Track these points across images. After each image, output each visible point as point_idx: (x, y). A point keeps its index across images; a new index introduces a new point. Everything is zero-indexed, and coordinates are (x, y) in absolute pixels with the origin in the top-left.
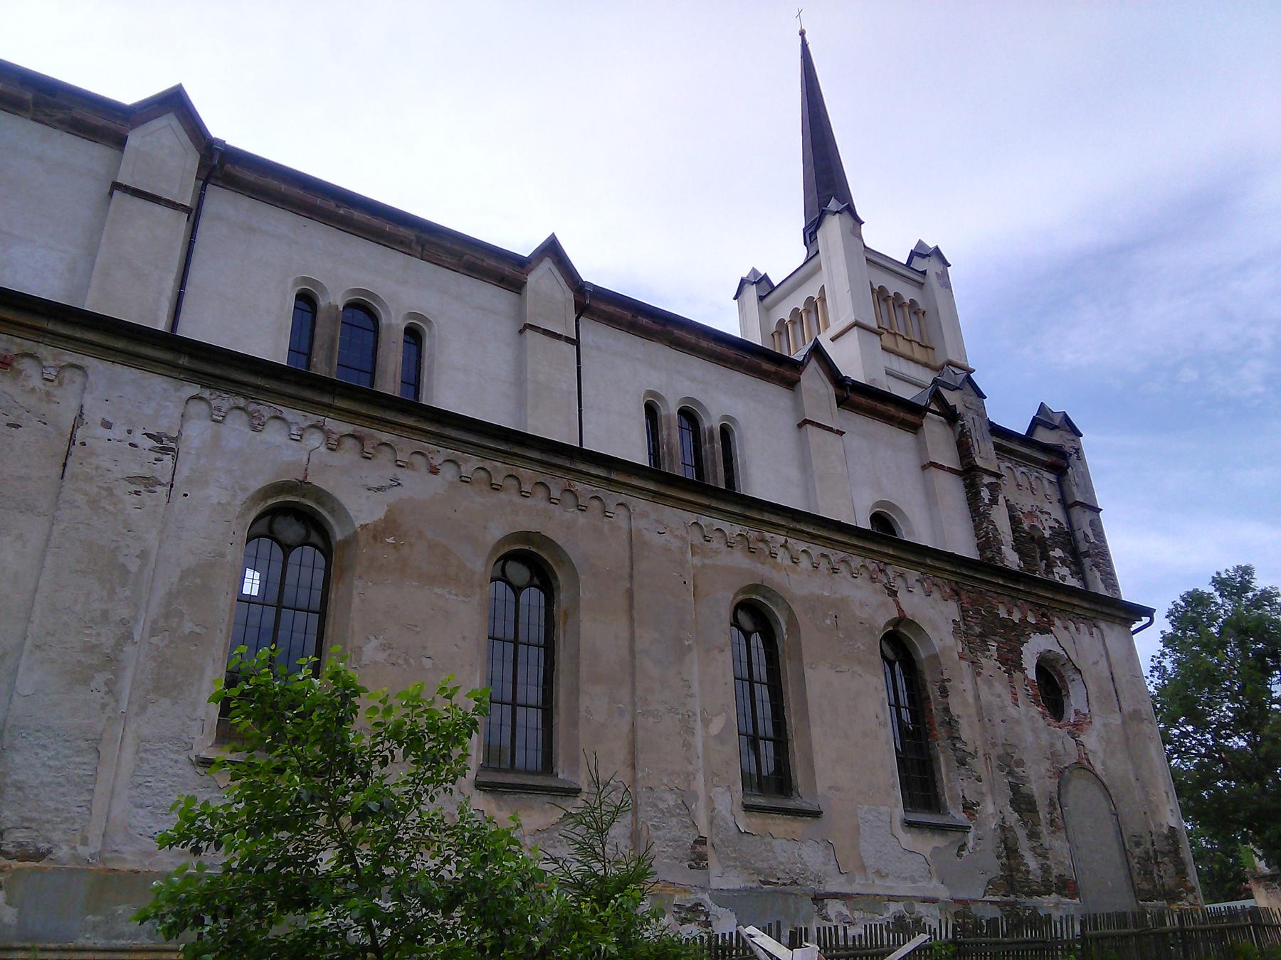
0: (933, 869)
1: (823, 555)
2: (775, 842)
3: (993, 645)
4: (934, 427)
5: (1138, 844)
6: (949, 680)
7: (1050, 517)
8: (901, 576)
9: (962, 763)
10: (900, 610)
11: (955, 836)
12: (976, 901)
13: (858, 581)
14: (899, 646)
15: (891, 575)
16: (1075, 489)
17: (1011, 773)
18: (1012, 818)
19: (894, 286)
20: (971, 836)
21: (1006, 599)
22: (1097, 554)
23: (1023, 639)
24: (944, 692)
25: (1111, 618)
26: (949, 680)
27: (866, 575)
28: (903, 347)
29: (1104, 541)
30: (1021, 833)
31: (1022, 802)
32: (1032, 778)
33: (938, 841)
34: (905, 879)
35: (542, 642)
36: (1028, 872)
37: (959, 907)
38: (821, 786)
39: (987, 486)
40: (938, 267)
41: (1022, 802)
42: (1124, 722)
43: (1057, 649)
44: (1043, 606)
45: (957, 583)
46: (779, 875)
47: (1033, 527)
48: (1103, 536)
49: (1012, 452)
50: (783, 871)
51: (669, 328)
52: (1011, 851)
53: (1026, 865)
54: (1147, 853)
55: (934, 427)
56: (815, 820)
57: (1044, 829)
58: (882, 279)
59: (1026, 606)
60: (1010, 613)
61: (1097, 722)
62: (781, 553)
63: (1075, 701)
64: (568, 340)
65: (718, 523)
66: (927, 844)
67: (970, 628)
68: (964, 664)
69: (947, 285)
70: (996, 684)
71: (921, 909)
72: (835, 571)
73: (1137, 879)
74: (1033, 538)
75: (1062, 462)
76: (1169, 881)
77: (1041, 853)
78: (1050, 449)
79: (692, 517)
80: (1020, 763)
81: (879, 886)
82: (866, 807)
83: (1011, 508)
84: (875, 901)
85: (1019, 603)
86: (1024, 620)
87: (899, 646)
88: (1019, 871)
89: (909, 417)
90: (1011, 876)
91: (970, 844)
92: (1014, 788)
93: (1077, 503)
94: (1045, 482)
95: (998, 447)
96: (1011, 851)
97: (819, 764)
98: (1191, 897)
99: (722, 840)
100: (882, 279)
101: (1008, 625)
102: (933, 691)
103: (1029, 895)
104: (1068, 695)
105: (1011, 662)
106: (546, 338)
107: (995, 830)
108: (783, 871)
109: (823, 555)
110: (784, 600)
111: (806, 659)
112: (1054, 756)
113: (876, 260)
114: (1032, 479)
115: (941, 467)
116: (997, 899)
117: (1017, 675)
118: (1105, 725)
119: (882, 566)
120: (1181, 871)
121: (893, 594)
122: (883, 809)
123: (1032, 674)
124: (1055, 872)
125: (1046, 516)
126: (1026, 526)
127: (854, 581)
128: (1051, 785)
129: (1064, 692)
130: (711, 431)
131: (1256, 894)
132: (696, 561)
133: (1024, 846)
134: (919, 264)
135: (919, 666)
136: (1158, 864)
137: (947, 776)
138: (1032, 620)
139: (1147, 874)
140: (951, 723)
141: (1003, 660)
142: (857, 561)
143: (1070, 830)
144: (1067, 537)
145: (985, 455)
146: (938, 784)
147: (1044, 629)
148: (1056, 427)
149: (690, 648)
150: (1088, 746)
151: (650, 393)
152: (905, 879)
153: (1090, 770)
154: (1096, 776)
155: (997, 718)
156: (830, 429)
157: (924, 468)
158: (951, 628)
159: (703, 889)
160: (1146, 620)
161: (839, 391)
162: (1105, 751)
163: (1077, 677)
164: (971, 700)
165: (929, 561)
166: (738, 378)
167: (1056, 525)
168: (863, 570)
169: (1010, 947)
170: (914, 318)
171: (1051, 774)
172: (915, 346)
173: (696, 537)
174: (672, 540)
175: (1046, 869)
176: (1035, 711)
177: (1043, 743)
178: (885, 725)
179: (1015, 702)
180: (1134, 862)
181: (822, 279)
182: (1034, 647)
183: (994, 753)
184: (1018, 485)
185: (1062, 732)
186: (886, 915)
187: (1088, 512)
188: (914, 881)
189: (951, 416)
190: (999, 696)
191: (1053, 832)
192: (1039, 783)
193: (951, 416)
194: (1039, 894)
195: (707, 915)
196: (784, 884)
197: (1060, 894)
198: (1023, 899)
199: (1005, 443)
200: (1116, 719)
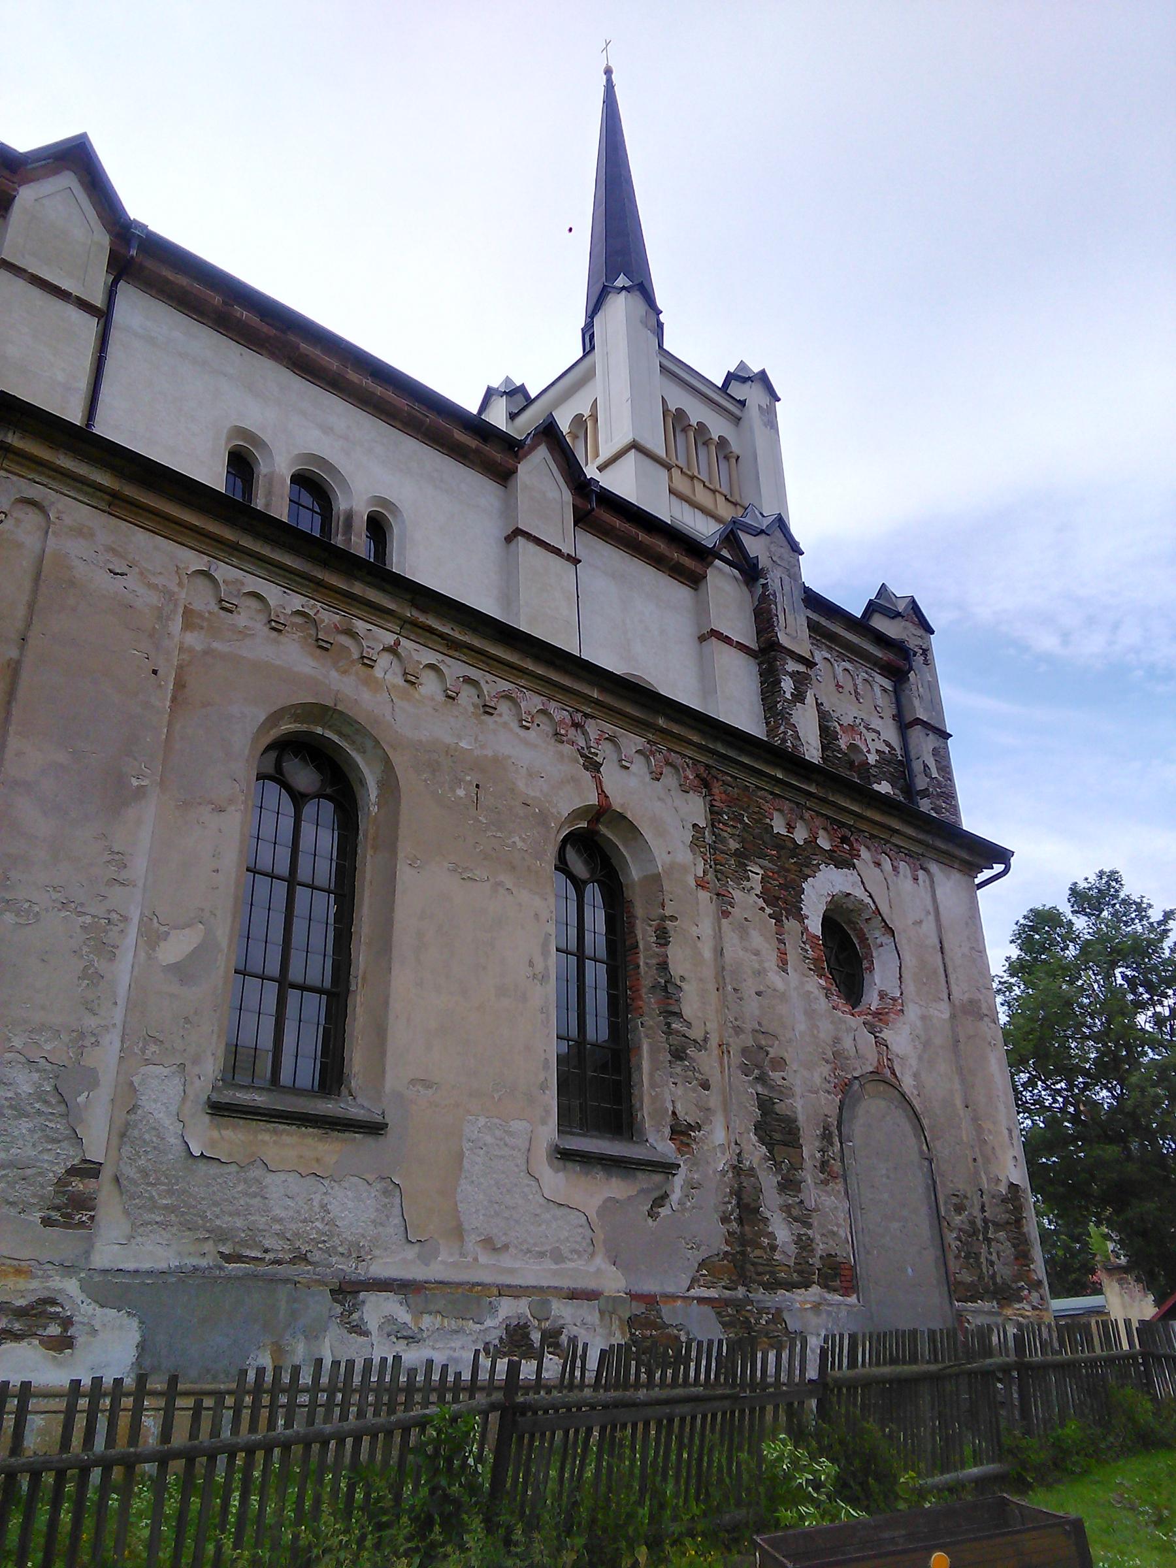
0: (600, 1235)
1: (468, 680)
2: (269, 1179)
3: (756, 873)
4: (722, 581)
5: (959, 1209)
6: (673, 918)
7: (878, 737)
8: (611, 739)
9: (678, 1055)
10: (602, 793)
11: (648, 1180)
12: (674, 1297)
13: (532, 735)
14: (594, 851)
15: (593, 734)
16: (916, 702)
17: (762, 1079)
18: (756, 1153)
19: (697, 413)
20: (678, 1181)
21: (787, 806)
22: (939, 795)
23: (807, 871)
24: (663, 937)
25: (947, 860)
26: (673, 918)
27: (547, 728)
28: (703, 496)
29: (951, 779)
30: (769, 1181)
31: (777, 1130)
32: (798, 1090)
33: (617, 1188)
34: (542, 1254)
35: (328, 984)
36: (773, 1248)
37: (638, 1308)
38: (394, 1080)
39: (792, 675)
40: (765, 400)
41: (777, 1130)
42: (953, 1016)
43: (859, 893)
44: (843, 825)
45: (707, 766)
46: (267, 1243)
47: (853, 747)
48: (950, 773)
49: (832, 637)
50: (280, 1235)
51: (292, 338)
52: (746, 1211)
53: (772, 1236)
54: (972, 1223)
55: (722, 581)
56: (370, 1142)
57: (809, 1176)
58: (679, 399)
59: (818, 822)
60: (790, 828)
61: (912, 1012)
62: (384, 660)
63: (881, 977)
64: (84, 305)
65: (253, 583)
66: (594, 1193)
67: (724, 841)
68: (704, 896)
69: (771, 423)
70: (754, 934)
71: (563, 1312)
72: (488, 710)
73: (953, 1265)
74: (852, 763)
75: (901, 663)
76: (1004, 1271)
77: (800, 1216)
78: (887, 642)
79: (197, 562)
80: (779, 1063)
81: (485, 1269)
82: (482, 1121)
83: (824, 717)
84: (466, 1298)
85: (807, 815)
86: (812, 842)
87: (594, 851)
88: (759, 1246)
89: (687, 561)
90: (743, 1253)
91: (676, 1196)
92: (765, 1105)
93: (918, 721)
94: (877, 689)
95: (813, 627)
96: (746, 1211)
97: (399, 1034)
98: (1035, 1296)
99: (145, 1173)
100: (679, 399)
101: (784, 845)
102: (644, 934)
103: (772, 1286)
104: (871, 969)
105: (783, 901)
106: (35, 292)
107: (724, 1173)
108: (280, 1235)
109: (468, 680)
110: (377, 742)
111: (405, 849)
112: (838, 1058)
113: (675, 371)
114: (859, 681)
115: (727, 640)
116: (712, 1293)
117: (791, 924)
118: (923, 1018)
119: (578, 717)
120: (1023, 1257)
121: (593, 766)
122: (517, 1125)
123: (815, 926)
124: (820, 1248)
125: (874, 736)
126: (843, 743)
127: (522, 732)
128: (828, 1104)
129: (865, 964)
130: (349, 517)
131: (1107, 1289)
132: (193, 639)
133: (771, 1201)
134: (737, 390)
135: (628, 894)
136: (988, 1241)
137: (651, 1075)
138: (824, 843)
139: (971, 1258)
140: (668, 989)
141: (769, 897)
142: (532, 702)
143: (852, 1180)
144: (900, 767)
145: (793, 631)
146: (635, 1091)
147: (844, 862)
148: (899, 615)
149: (140, 793)
150: (894, 1048)
151: (241, 432)
152: (542, 1254)
153: (893, 1084)
154: (903, 1095)
155: (749, 987)
156: (557, 552)
157: (702, 639)
158: (688, 836)
159: (68, 1269)
160: (999, 868)
161: (579, 502)
162: (920, 1058)
163: (886, 939)
164: (707, 954)
165: (661, 722)
166: (411, 446)
167: (887, 750)
168: (541, 719)
169: (649, 1411)
170: (723, 465)
171: (830, 1087)
172: (720, 499)
173: (202, 600)
174: (141, 590)
175: (804, 1245)
176: (815, 984)
177: (822, 1035)
178: (544, 978)
179: (783, 965)
180: (951, 1237)
181: (595, 390)
182: (822, 887)
183: (736, 1044)
184: (838, 685)
185: (855, 1022)
186: (489, 1323)
187: (931, 736)
188: (558, 1257)
189: (750, 572)
190: (757, 953)
191: (825, 1182)
192: (808, 1097)
193: (750, 572)
194: (790, 1286)
195: (67, 1322)
196: (278, 1262)
197: (825, 1286)
198: (759, 1295)
199: (823, 621)
200: (941, 1012)
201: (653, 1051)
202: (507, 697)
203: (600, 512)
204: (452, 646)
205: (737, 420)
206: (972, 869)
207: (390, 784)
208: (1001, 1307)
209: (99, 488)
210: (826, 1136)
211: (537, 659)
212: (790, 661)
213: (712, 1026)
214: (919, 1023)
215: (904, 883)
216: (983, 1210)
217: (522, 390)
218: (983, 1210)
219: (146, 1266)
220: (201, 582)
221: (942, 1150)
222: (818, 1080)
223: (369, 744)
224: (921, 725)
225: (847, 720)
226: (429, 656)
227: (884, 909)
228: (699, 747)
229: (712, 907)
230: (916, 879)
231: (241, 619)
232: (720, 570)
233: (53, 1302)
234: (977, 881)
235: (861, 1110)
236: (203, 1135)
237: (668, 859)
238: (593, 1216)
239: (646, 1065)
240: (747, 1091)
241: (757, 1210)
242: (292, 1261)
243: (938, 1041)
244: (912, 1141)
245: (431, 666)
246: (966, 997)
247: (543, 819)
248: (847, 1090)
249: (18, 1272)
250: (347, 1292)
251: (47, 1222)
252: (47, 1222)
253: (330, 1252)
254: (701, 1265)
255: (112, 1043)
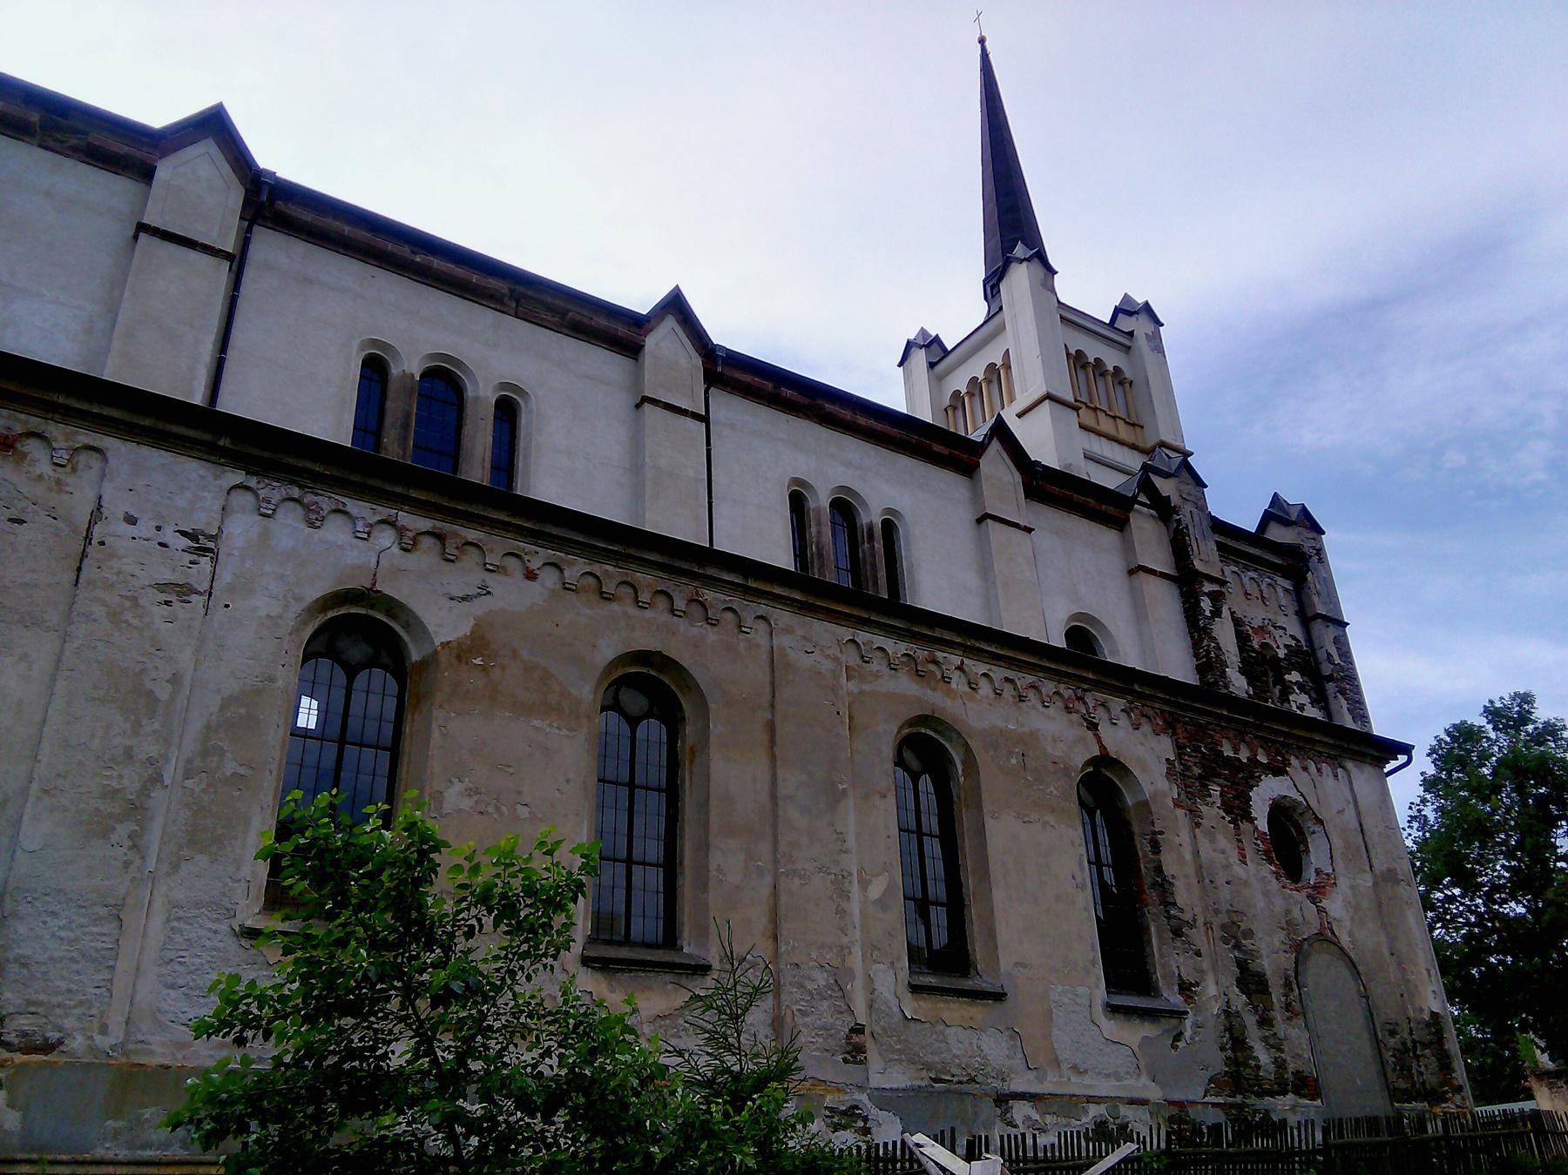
1: (1007, 680)
2: (948, 1031)
3: (1215, 790)
4: (1144, 525)
5: (1393, 1033)
6: (1161, 833)
7: (1286, 633)
9: (1177, 933)
10: (1102, 747)
12: (1194, 1103)
13: (1051, 711)
14: (1102, 787)
15: (1091, 704)
16: (1315, 599)
17: (1237, 946)
18: (1239, 1001)
19: (1094, 350)
20: (1188, 1023)
22: (1343, 679)
24: (1156, 847)
25: (1359, 757)
26: (1161, 833)
27: (1060, 704)
28: (1106, 425)
29: (1352, 663)
30: (1250, 1020)
31: (1251, 982)
32: (1264, 952)
33: (1148, 1030)
34: (1108, 1075)
36: (1258, 1067)
37: (1175, 1111)
39: (1209, 595)
40: (1149, 327)
41: (1251, 982)
42: (1375, 884)
43: (1293, 794)
45: (1171, 713)
46: (954, 1071)
47: (1264, 645)
48: (1350, 657)
50: (959, 1066)
51: (820, 402)
52: (1238, 1042)
53: (1256, 1058)
54: (1404, 1043)
55: (1144, 525)
57: (1278, 1015)
58: (1079, 342)
60: (1236, 751)
61: (1343, 884)
63: (1316, 857)
64: (695, 416)
66: (1135, 1033)
68: (1180, 812)
69: (1159, 349)
70: (1220, 837)
71: (1127, 1112)
72: (1021, 699)
73: (1391, 1076)
76: (1431, 1079)
77: (1275, 1044)
78: (1285, 549)
80: (1249, 934)
81: (1076, 1085)
83: (1237, 622)
84: (1070, 1103)
86: (1253, 760)
87: (1102, 787)
88: (1247, 1066)
89: (1112, 510)
90: (1238, 1072)
91: (1188, 1033)
92: (1242, 965)
94: (1280, 590)
97: (1003, 935)
98: (1457, 1098)
99: (883, 1028)
100: (1079, 342)
101: (1233, 765)
102: (1142, 846)
103: (1261, 1094)
104: (1307, 851)
105: (1238, 809)
107: (1218, 1016)
108: (959, 1066)
112: (1290, 926)
113: (1072, 319)
114: (1263, 586)
116: (1220, 1100)
117: (1245, 826)
118: (1352, 887)
121: (1093, 726)
122: (1081, 990)
123: (1263, 824)
124: (1291, 1067)
125: (1281, 632)
128: (1287, 961)
129: (1302, 847)
130: (871, 528)
132: (852, 686)
133: (1254, 1036)
134: (1125, 323)
136: (1417, 1057)
137: (1160, 949)
139: (1404, 1070)
140: (1164, 887)
141: (1227, 807)
142: (1049, 687)
145: (1206, 557)
147: (1279, 771)
152: (1108, 1075)
153: (1334, 942)
154: (1342, 949)
155: (1221, 879)
156: (1016, 525)
157: (1131, 572)
159: (861, 1088)
160: (1402, 759)
162: (1352, 920)
163: (1317, 828)
164: (1188, 856)
166: (904, 462)
167: (1293, 643)
168: (1056, 698)
170: (1119, 390)
173: (851, 657)
174: (823, 661)
175: (1280, 1064)
176: (1268, 870)
177: (1277, 909)
178: (1083, 888)
179: (1243, 859)
180: (1388, 1055)
181: (1006, 342)
182: (1265, 792)
183: (1217, 921)
184: (1246, 594)
185: (1300, 896)
186: (1084, 1120)
188: (1119, 1078)
189: (1164, 509)
190: (1223, 852)
191: (1289, 1019)
192: (1272, 959)
193: (1164, 509)
194: (1272, 1094)
195: (866, 1119)
196: (960, 1082)
197: (1297, 1093)
198: (1252, 1100)
199: (1230, 543)
200: (1366, 881)
201: (1159, 931)
202: (1032, 686)
203: (1048, 487)
204: (995, 658)
205: (1127, 349)
206: (1380, 762)
207: (970, 762)
208: (1431, 1106)
209: (794, 600)
210: (1287, 985)
211: (1050, 659)
212: (1206, 584)
213: (1198, 910)
214: (1349, 892)
215: (1328, 782)
216: (1411, 1033)
217: (937, 340)
218: (1411, 1033)
219: (895, 1086)
220: (852, 647)
221: (1376, 990)
222: (1277, 944)
223: (954, 735)
224: (1320, 617)
225: (1257, 623)
226: (982, 668)
227: (1313, 804)
228: (1166, 702)
229: (1187, 820)
230: (1336, 776)
231: (874, 666)
232: (1139, 512)
233: (857, 1107)
234: (1388, 768)
235: (1311, 963)
236: (911, 1006)
237: (1152, 788)
238: (1137, 1050)
239: (1154, 942)
240: (1229, 955)
241: (1244, 1041)
242: (968, 1082)
243: (1365, 904)
244: (1351, 984)
245: (984, 675)
246: (1384, 868)
247: (1066, 771)
248: (1299, 950)
249: (839, 1090)
250: (1003, 1100)
251: (845, 1061)
252: (845, 1061)
253: (986, 1076)
254: (1210, 1081)
255: (857, 951)
